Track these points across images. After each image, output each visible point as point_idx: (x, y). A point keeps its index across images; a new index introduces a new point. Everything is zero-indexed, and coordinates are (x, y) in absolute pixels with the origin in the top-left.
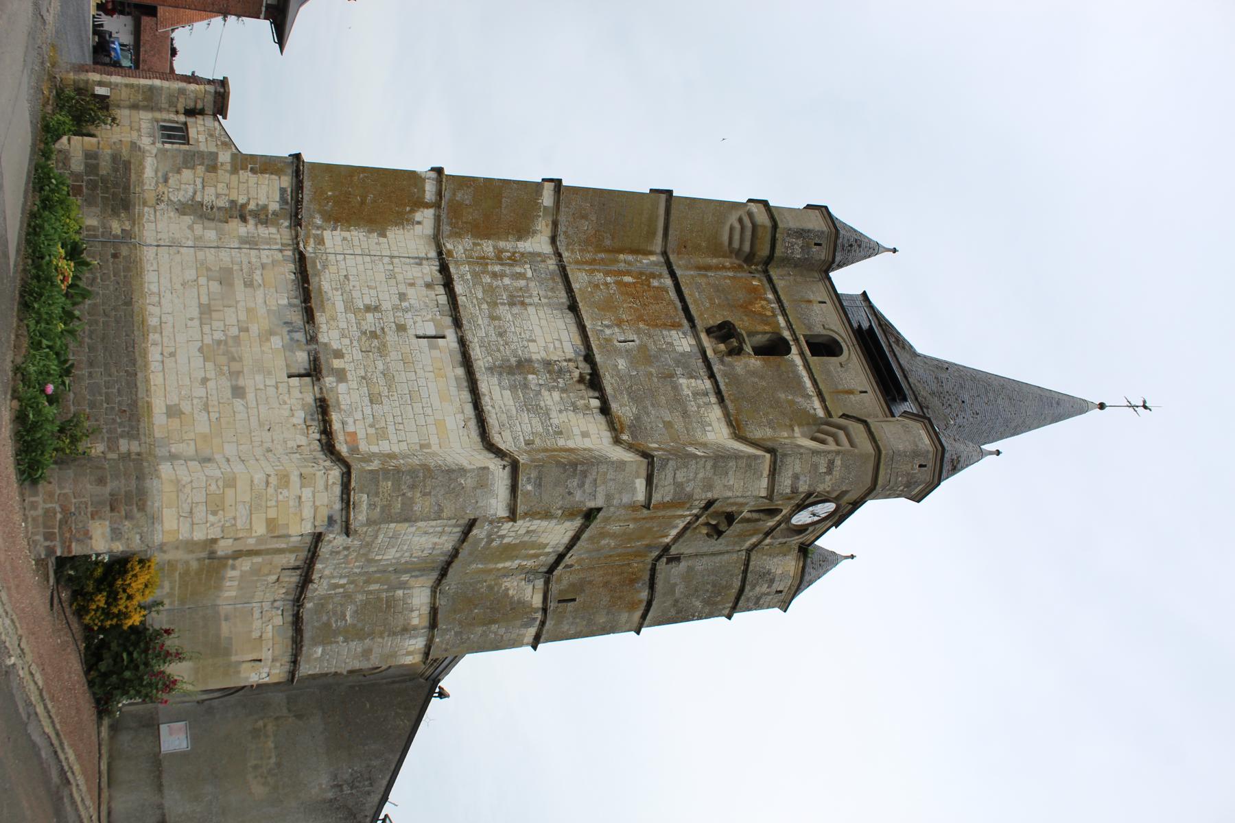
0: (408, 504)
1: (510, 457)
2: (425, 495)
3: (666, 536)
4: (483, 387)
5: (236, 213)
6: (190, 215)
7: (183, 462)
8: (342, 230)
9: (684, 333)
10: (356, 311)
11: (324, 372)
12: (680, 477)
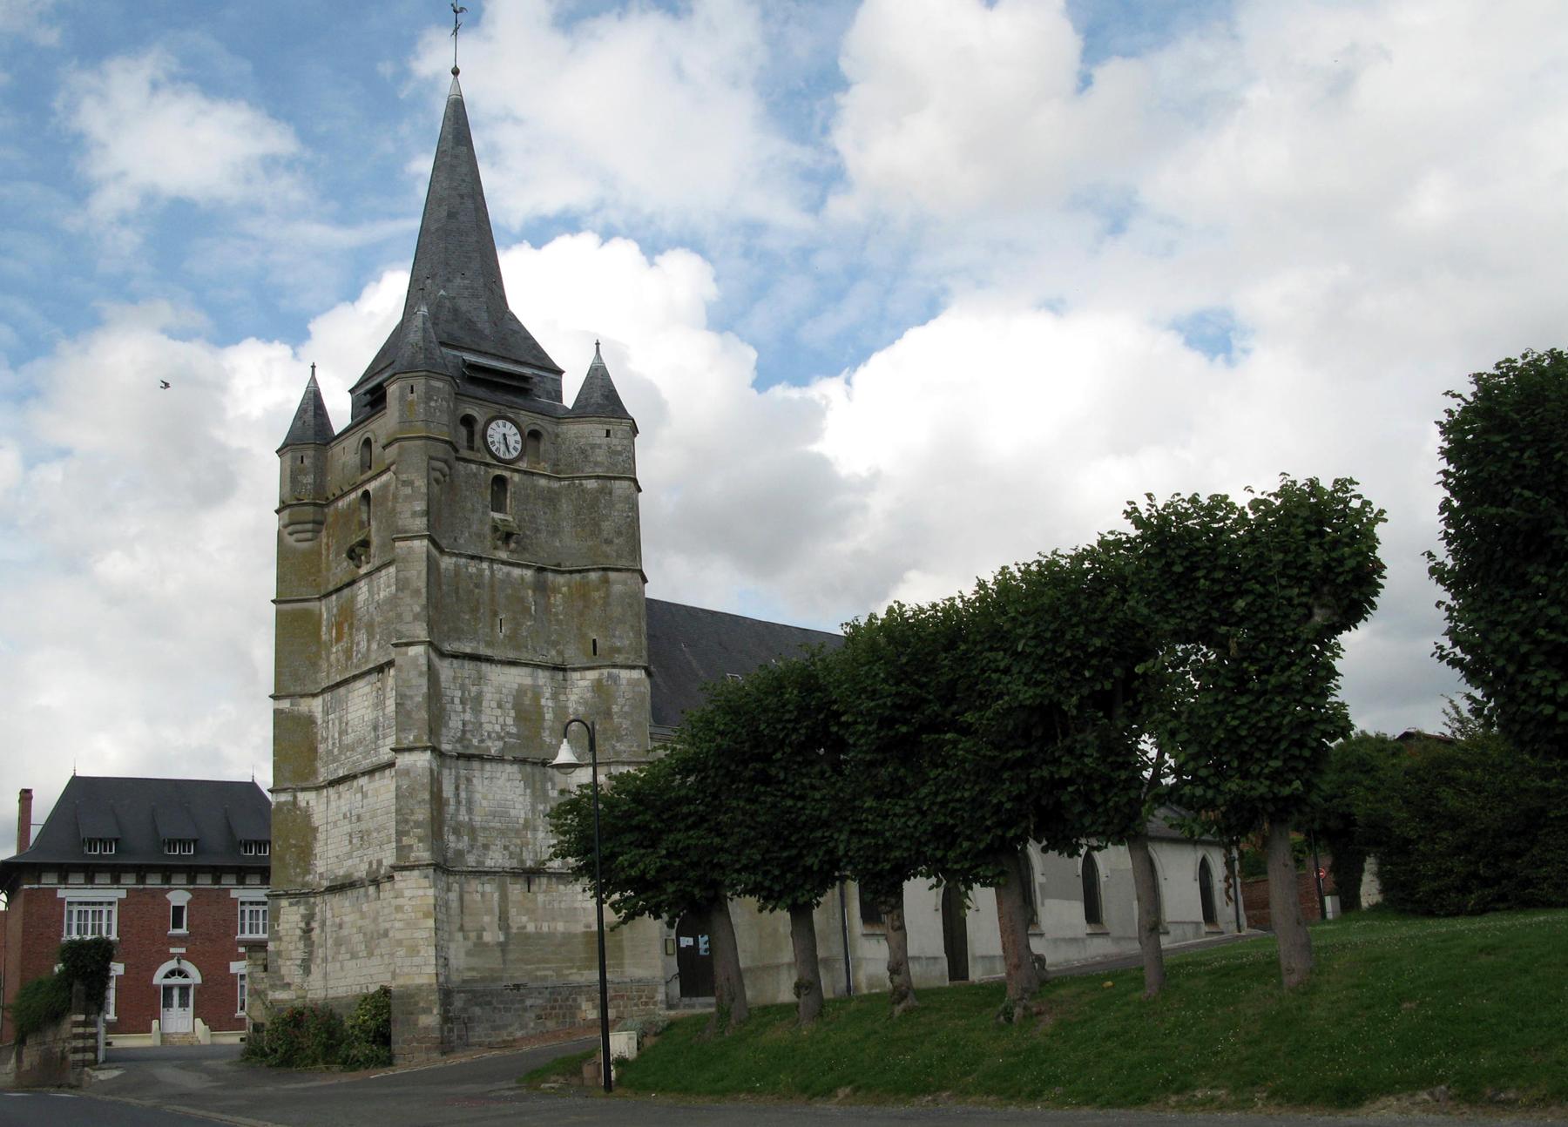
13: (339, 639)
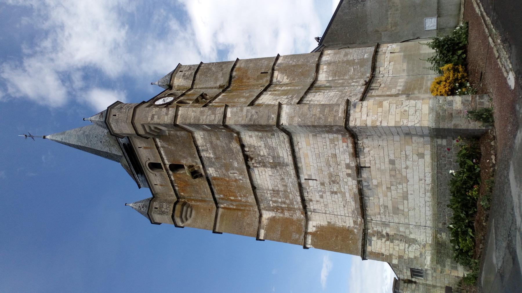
0: (322, 111)
1: (279, 128)
2: (315, 115)
3: (223, 96)
4: (290, 158)
5: (391, 237)
6: (411, 238)
7: (418, 134)
8: (346, 226)
9: (211, 175)
10: (341, 192)
11: (355, 168)
12: (213, 117)
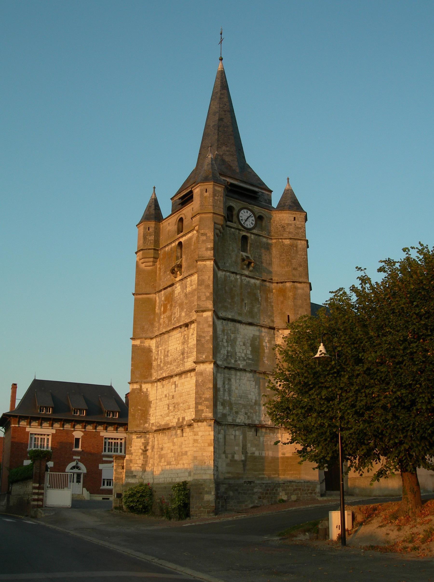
11: (191, 423)
13: (164, 312)
